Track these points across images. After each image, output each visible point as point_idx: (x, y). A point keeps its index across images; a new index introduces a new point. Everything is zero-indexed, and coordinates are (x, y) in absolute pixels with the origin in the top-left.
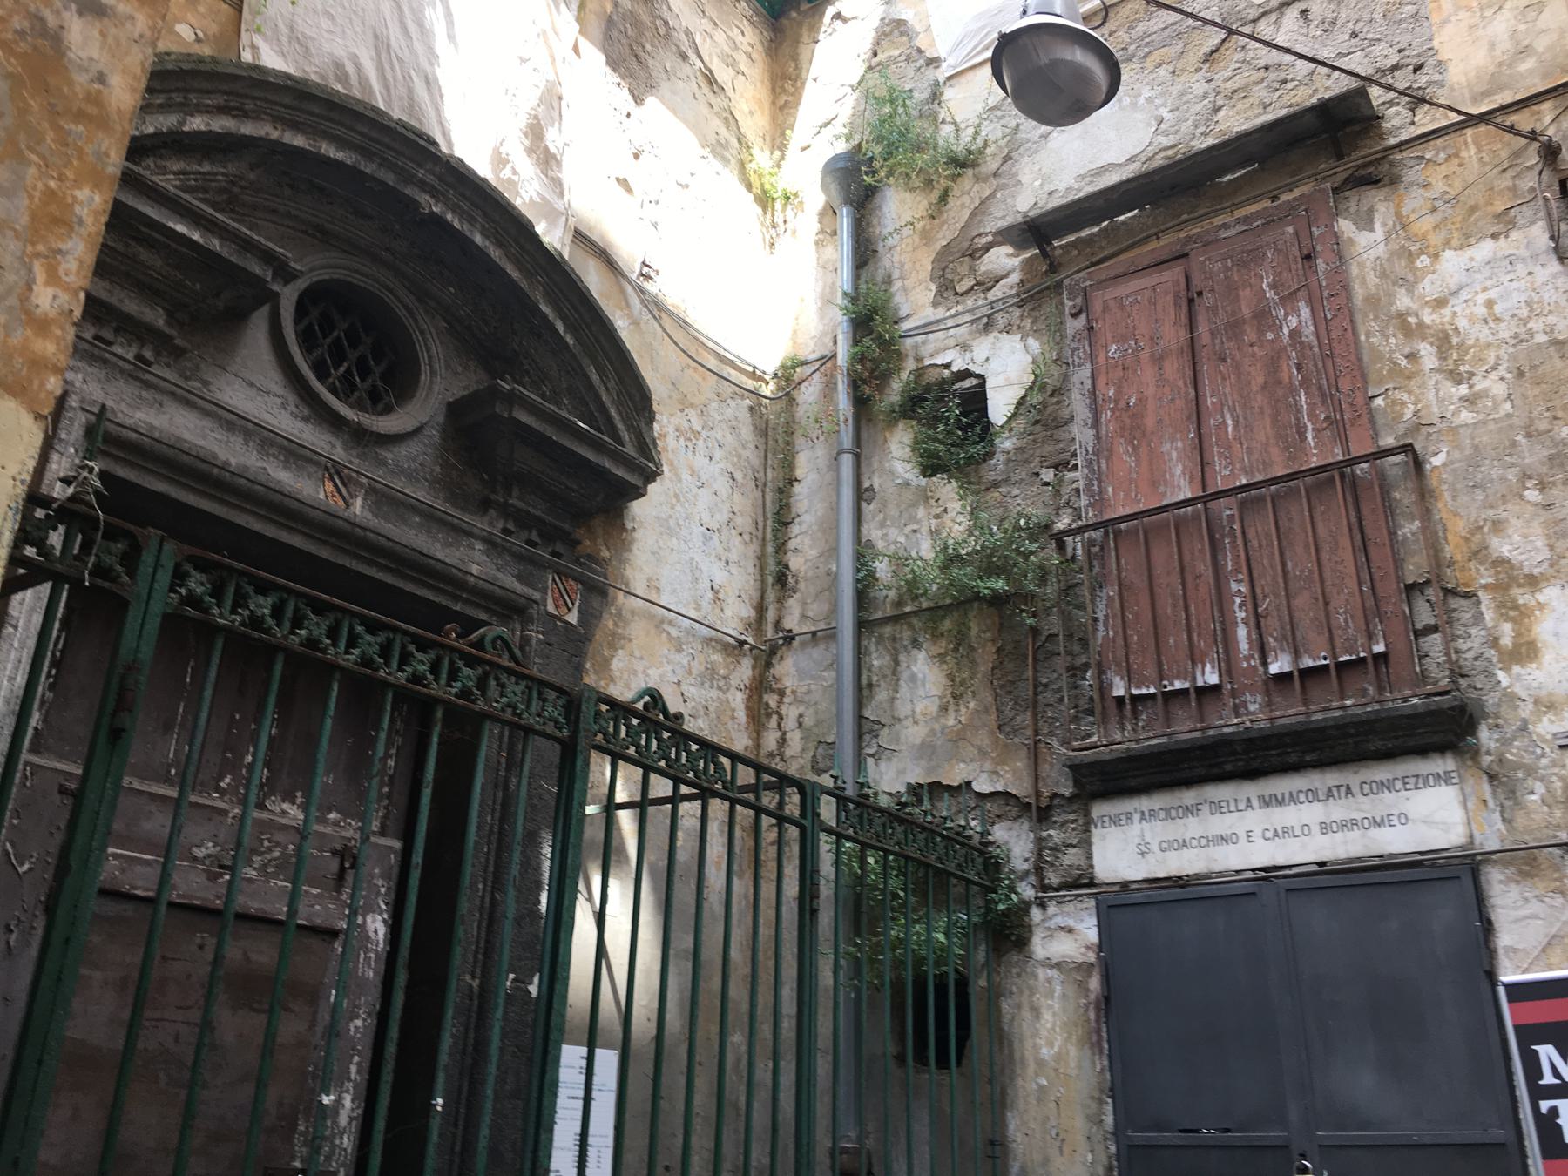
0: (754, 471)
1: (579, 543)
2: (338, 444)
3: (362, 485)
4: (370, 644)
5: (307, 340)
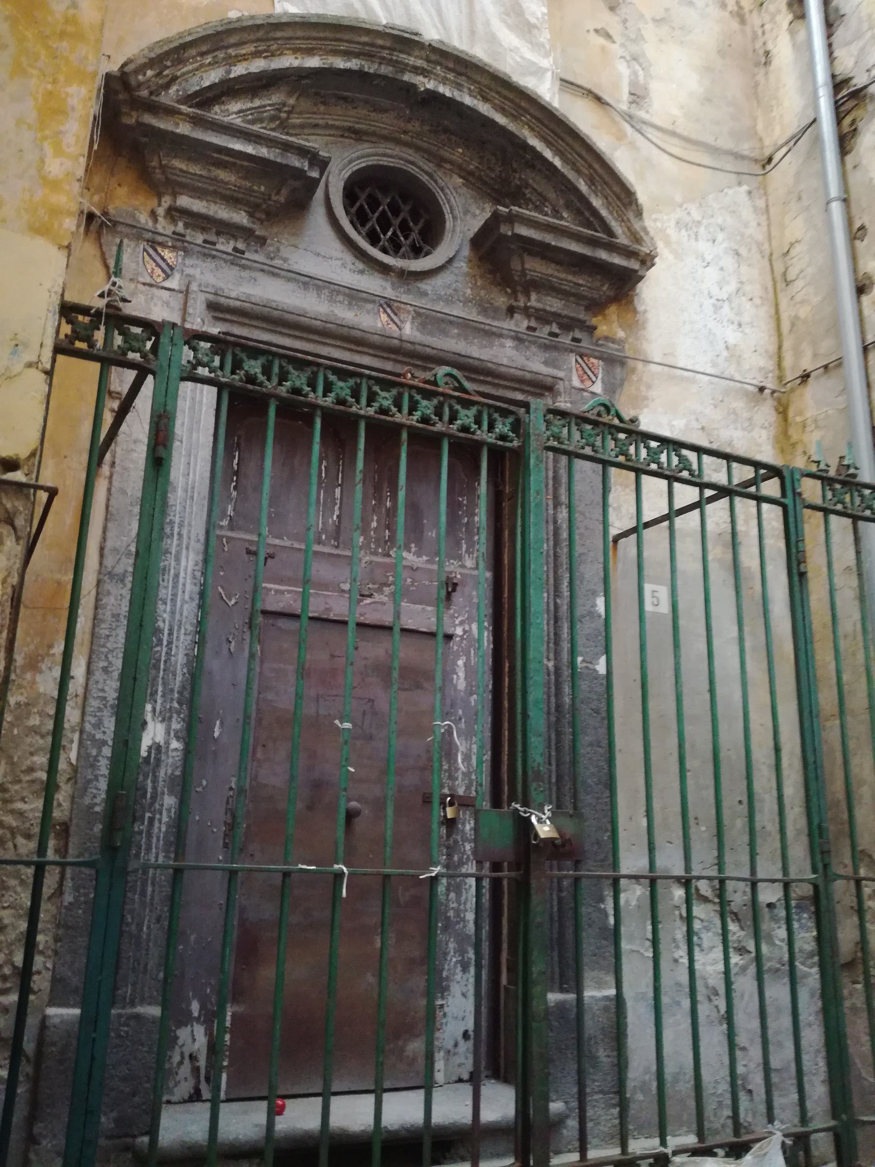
0: (759, 245)
1: (595, 328)
2: (388, 285)
3: (409, 312)
4: (341, 388)
5: (359, 219)
